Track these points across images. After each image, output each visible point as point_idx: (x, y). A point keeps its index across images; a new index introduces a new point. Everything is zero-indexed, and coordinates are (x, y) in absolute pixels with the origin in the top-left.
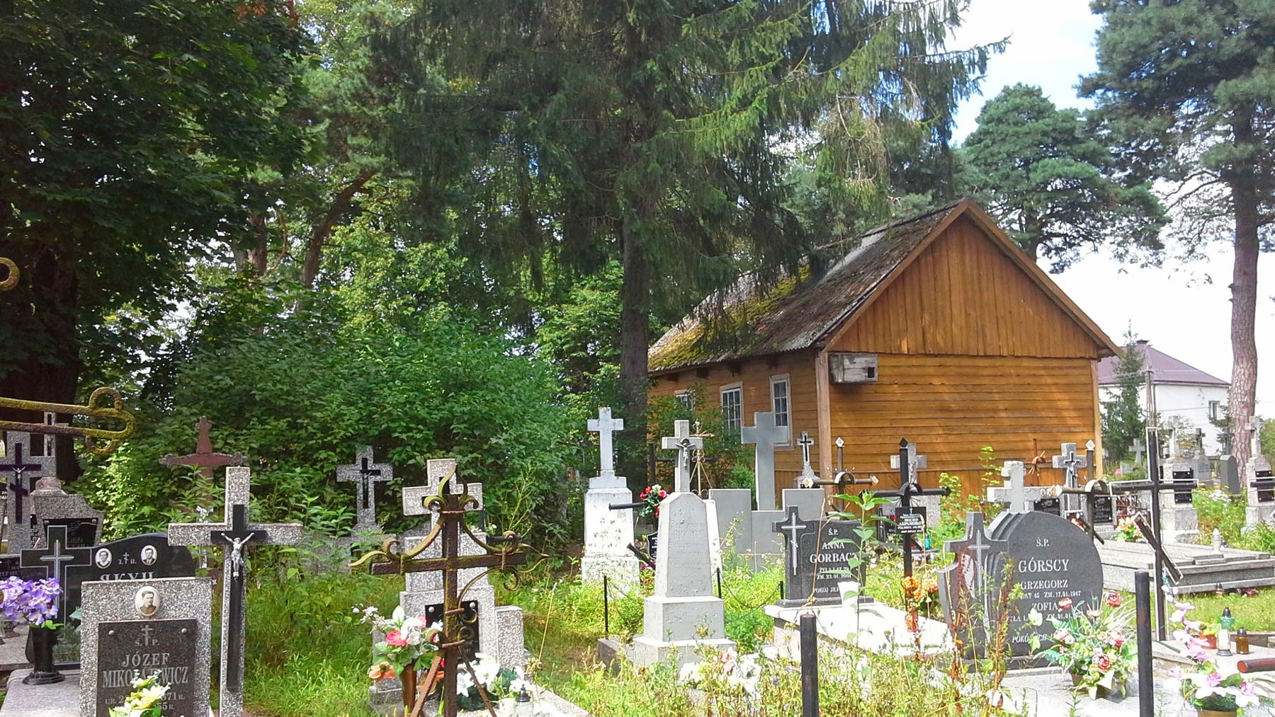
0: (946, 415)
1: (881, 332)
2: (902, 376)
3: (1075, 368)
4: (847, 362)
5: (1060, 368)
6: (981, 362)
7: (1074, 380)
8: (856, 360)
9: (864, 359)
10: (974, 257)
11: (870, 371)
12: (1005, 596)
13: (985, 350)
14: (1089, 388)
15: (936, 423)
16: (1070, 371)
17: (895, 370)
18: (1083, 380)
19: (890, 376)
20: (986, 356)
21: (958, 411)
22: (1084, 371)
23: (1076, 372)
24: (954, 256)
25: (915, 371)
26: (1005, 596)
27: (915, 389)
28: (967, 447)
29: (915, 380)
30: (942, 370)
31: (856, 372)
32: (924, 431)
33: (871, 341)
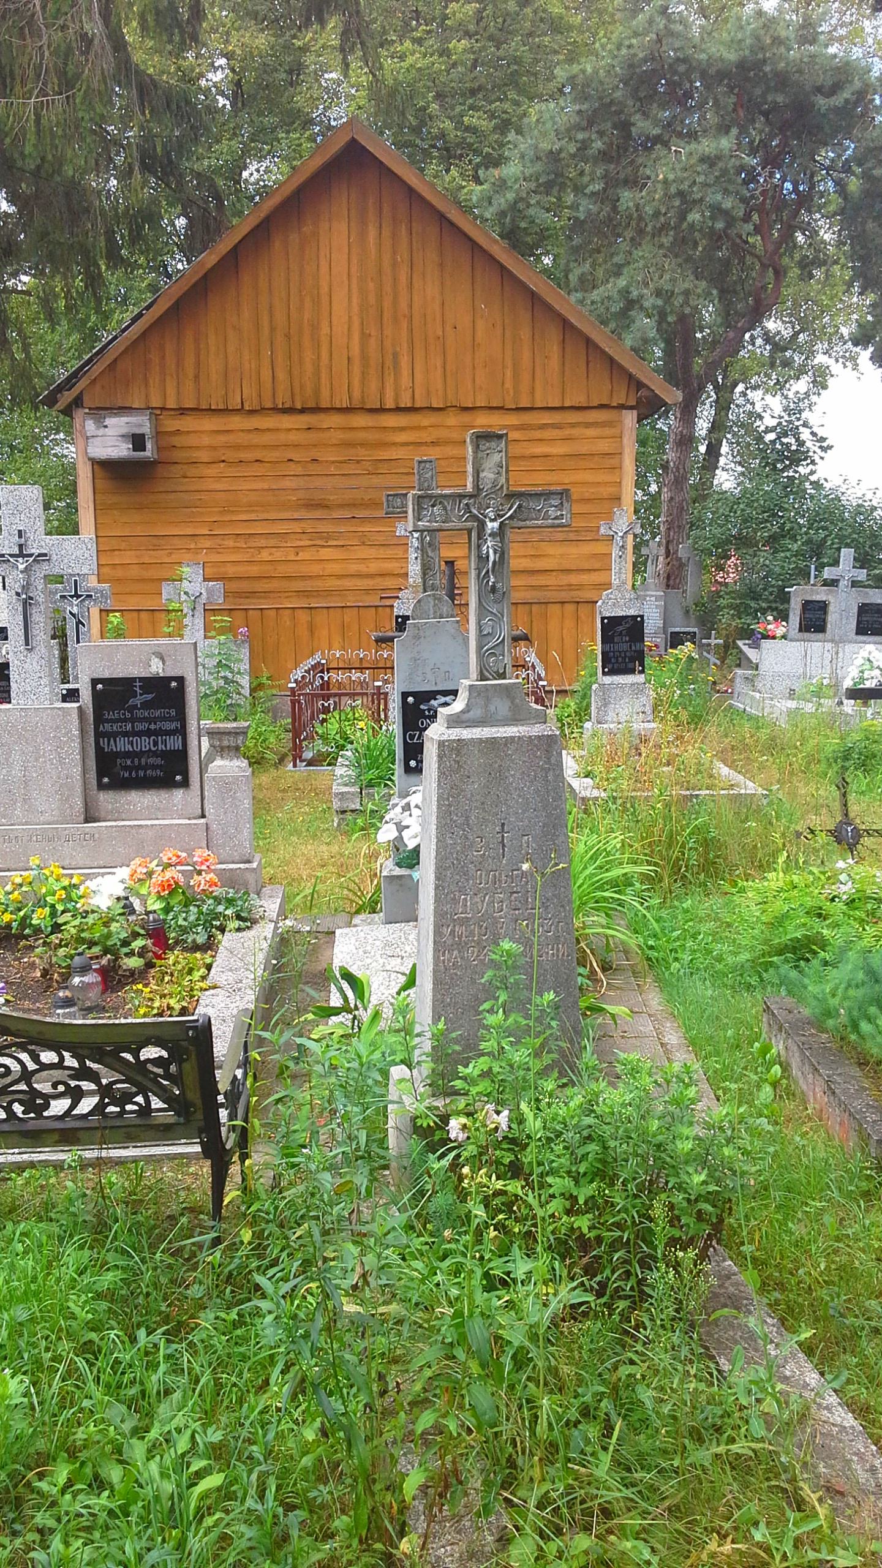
0: (318, 514)
1: (190, 371)
2: (237, 447)
3: (588, 425)
4: (90, 426)
5: (553, 426)
6: (391, 420)
7: (584, 449)
8: (108, 421)
9: (125, 419)
10: (386, 232)
11: (138, 442)
12: (533, 1433)
13: (397, 397)
14: (614, 462)
15: (296, 527)
16: (576, 432)
17: (222, 439)
18: (604, 446)
19: (214, 448)
20: (398, 409)
21: (341, 506)
22: (608, 431)
23: (591, 432)
24: (343, 226)
25: (256, 439)
26: (533, 1433)
27: (258, 470)
28: (354, 568)
29: (258, 455)
30: (312, 436)
31: (111, 441)
32: (272, 542)
33: (171, 391)
